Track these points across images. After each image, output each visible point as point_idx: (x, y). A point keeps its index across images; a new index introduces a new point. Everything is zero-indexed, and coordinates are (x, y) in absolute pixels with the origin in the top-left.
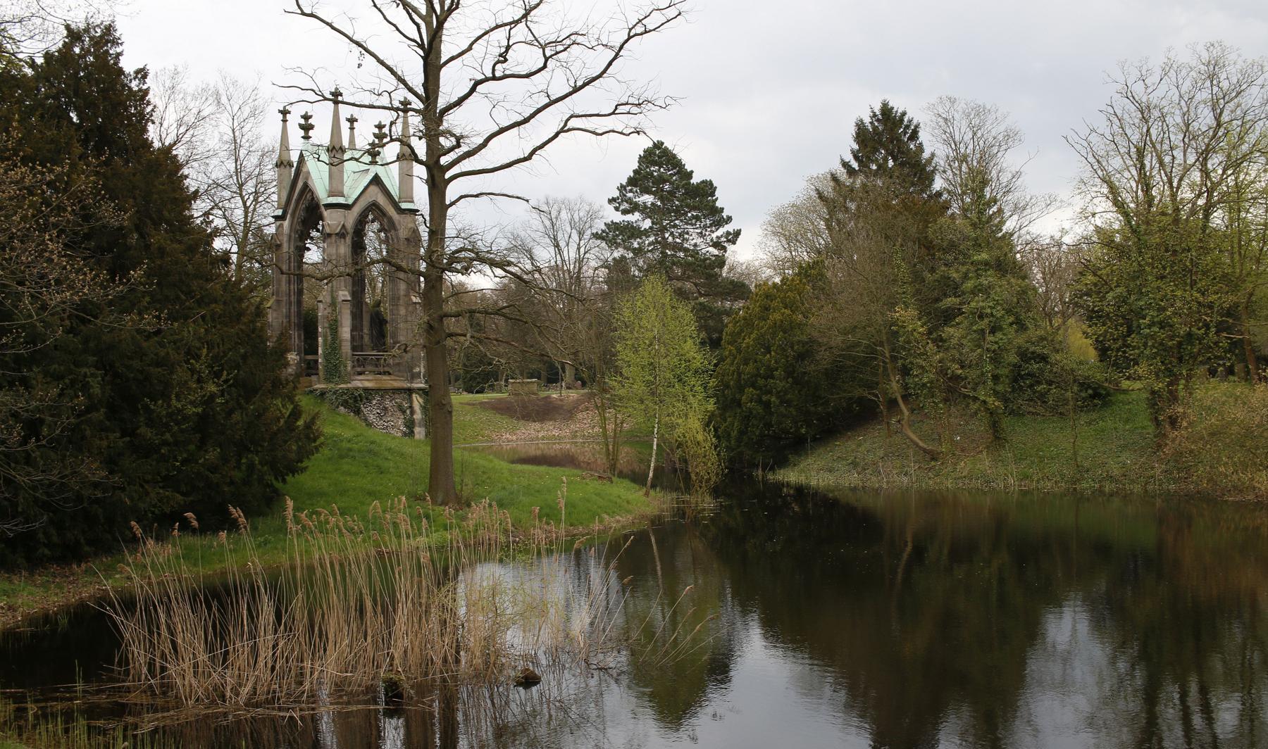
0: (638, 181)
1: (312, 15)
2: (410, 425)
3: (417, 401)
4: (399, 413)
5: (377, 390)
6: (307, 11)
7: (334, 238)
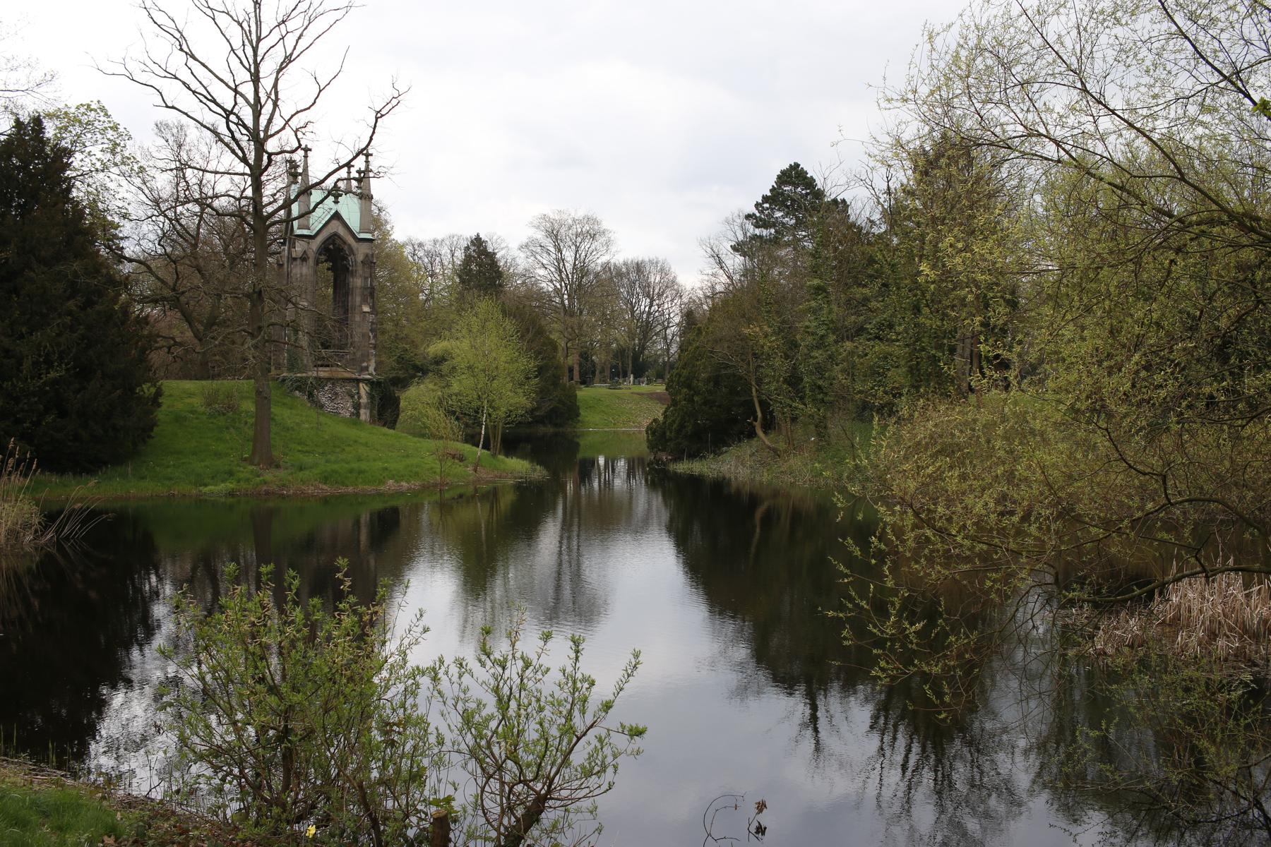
0: (775, 198)
1: (173, 107)
2: (357, 407)
3: (364, 389)
4: (347, 397)
5: (329, 379)
6: (170, 105)
7: (299, 261)
